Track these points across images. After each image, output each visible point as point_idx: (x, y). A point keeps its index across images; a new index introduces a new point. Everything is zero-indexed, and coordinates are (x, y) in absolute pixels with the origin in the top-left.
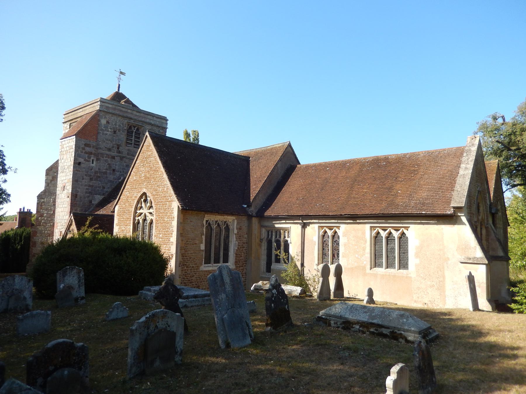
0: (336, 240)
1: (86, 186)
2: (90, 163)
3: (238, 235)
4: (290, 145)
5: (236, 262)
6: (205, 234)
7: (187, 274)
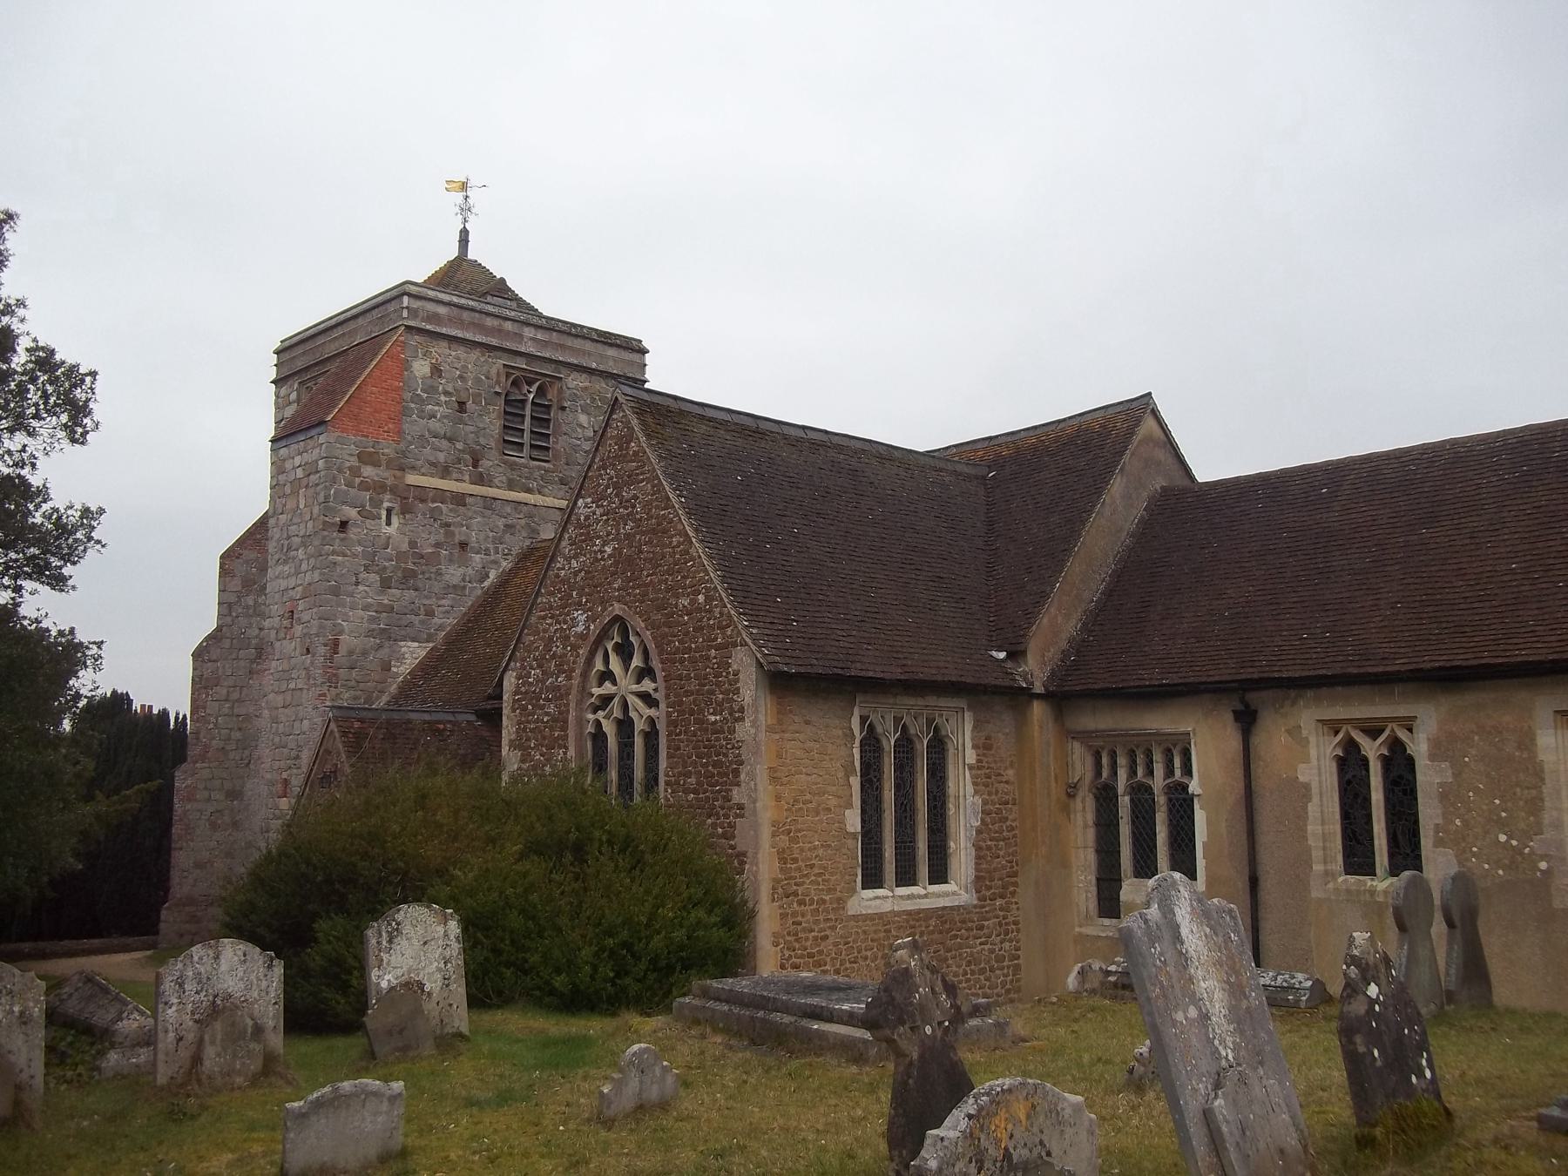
0: (1401, 777)
3: (979, 772)
5: (980, 882)
6: (858, 769)
7: (804, 930)
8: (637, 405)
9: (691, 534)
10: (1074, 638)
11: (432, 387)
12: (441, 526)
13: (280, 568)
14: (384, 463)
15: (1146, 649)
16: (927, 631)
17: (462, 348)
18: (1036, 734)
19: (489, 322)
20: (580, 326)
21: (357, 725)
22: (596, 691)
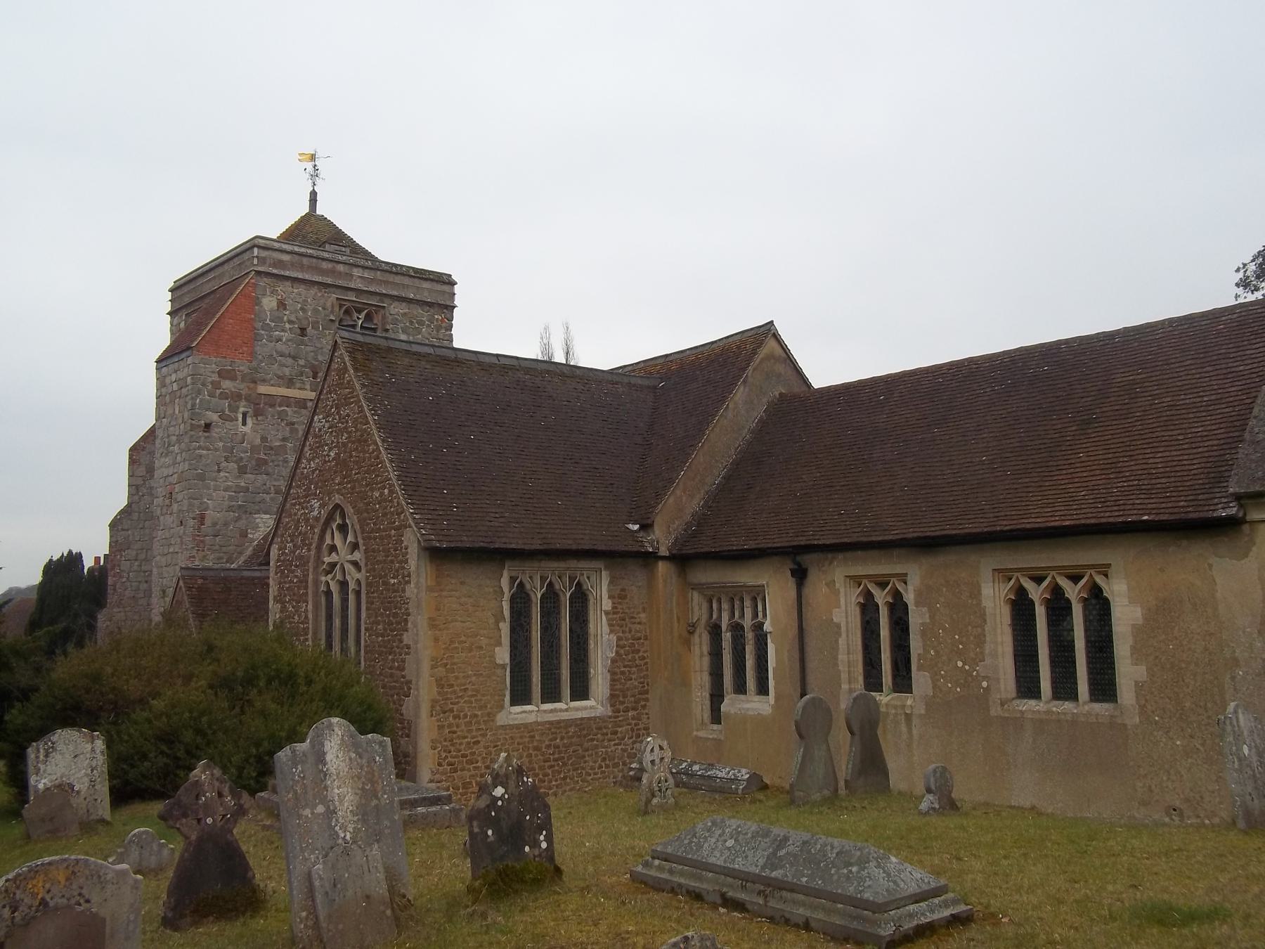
2: (238, 425)
3: (615, 616)
7: (459, 737)
8: (351, 346)
9: (380, 444)
10: (697, 512)
11: (279, 317)
12: (287, 425)
13: (163, 460)
14: (240, 378)
15: (742, 521)
16: (573, 511)
17: (302, 286)
18: (661, 586)
19: (325, 265)
20: (400, 265)
21: (200, 581)
22: (327, 560)
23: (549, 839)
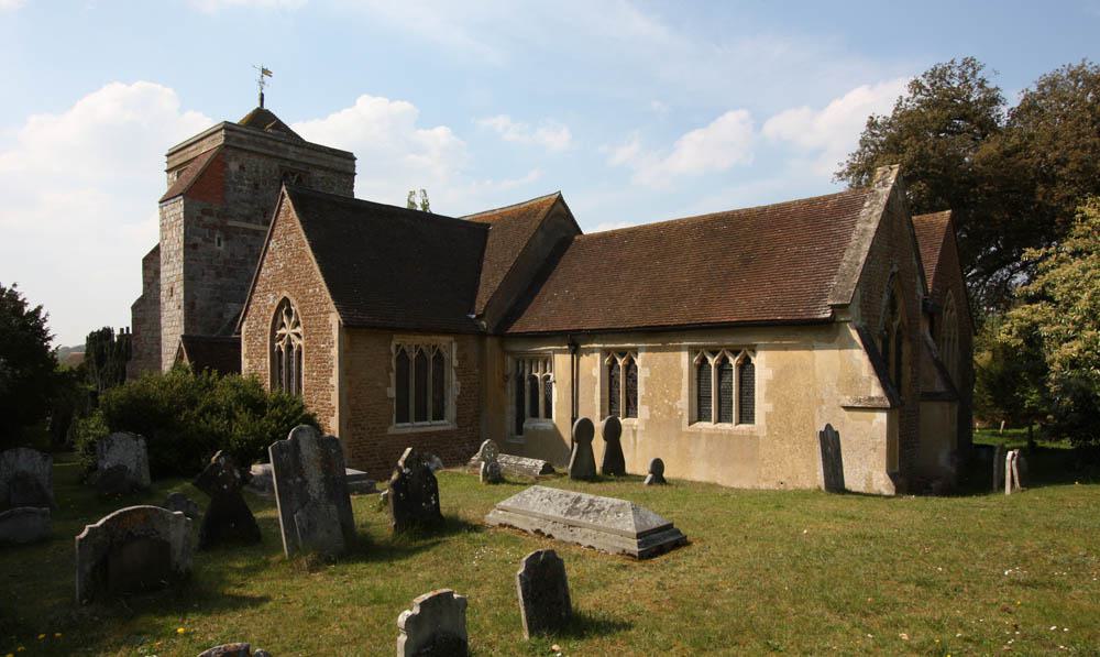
1: (209, 286)
4: (560, 199)
5: (458, 419)
6: (394, 368)
23: (437, 499)
